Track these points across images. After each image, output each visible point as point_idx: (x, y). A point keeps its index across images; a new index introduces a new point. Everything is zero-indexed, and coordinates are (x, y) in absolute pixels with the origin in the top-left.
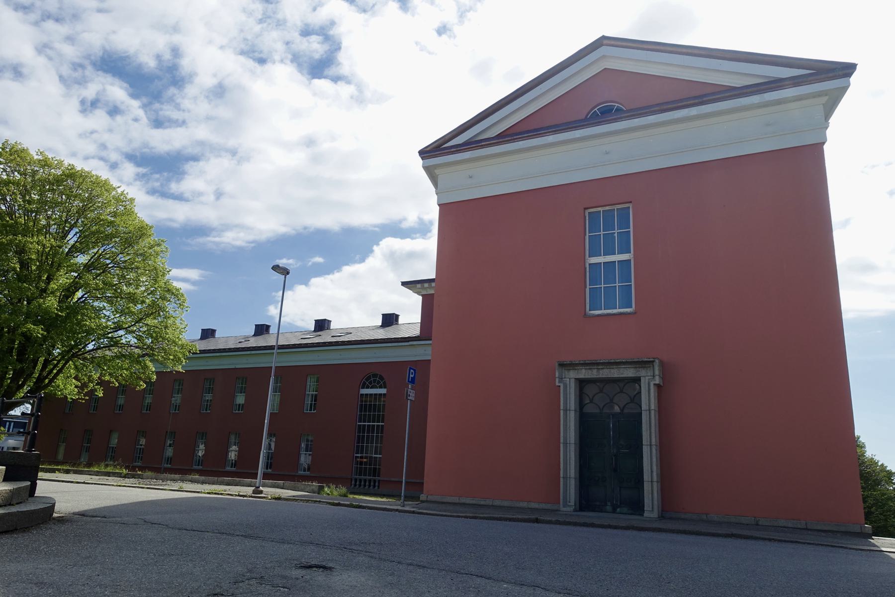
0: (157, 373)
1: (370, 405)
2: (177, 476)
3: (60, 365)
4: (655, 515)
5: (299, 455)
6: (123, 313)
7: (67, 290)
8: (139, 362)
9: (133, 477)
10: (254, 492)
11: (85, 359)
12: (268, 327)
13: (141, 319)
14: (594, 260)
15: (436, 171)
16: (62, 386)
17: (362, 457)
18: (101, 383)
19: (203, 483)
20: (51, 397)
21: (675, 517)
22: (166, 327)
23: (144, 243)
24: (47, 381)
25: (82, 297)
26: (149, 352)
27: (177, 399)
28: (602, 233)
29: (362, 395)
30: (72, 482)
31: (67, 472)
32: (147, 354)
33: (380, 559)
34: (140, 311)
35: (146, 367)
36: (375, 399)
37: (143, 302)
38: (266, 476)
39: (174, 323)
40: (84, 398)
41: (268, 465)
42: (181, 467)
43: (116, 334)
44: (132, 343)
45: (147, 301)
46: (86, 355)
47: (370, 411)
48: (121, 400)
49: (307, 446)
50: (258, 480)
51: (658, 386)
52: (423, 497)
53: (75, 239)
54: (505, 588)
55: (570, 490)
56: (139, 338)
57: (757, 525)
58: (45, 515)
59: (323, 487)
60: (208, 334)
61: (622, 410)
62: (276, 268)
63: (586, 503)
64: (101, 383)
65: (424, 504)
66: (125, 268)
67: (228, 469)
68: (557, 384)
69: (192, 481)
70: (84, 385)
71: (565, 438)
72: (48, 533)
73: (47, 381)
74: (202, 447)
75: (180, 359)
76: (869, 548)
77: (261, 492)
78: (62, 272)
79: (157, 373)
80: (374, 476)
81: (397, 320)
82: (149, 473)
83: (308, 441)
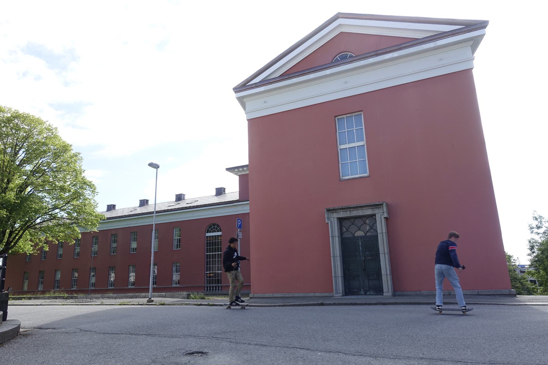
1: (213, 242)
2: (99, 295)
4: (390, 294)
6: (57, 199)
7: (21, 187)
8: (69, 228)
9: (72, 298)
10: (148, 302)
12: (147, 201)
13: (69, 202)
14: (342, 147)
15: (244, 100)
17: (210, 273)
18: (47, 242)
19: (115, 298)
20: (16, 253)
22: (85, 205)
23: (67, 156)
24: (12, 244)
25: (31, 191)
26: (76, 221)
27: (95, 248)
28: (346, 130)
29: (207, 237)
30: (33, 305)
31: (30, 298)
36: (215, 238)
37: (69, 191)
38: (155, 290)
39: (90, 203)
40: (36, 253)
42: (102, 289)
43: (54, 212)
44: (64, 216)
45: (72, 190)
46: (36, 226)
47: (213, 246)
48: (61, 252)
49: (177, 269)
50: (150, 294)
51: (386, 219)
52: (251, 295)
53: (23, 155)
54: (321, 355)
55: (339, 284)
56: (69, 213)
57: (450, 295)
60: (111, 208)
61: (366, 234)
62: (151, 165)
63: (348, 291)
64: (47, 242)
65: (252, 300)
66: (57, 171)
67: (130, 287)
68: (327, 222)
69: (108, 298)
71: (334, 253)
72: (16, 345)
73: (12, 244)
74: (113, 275)
75: (95, 224)
76: (518, 303)
77: (152, 301)
78: (16, 176)
80: (218, 283)
81: (224, 191)
82: (81, 295)
83: (177, 266)
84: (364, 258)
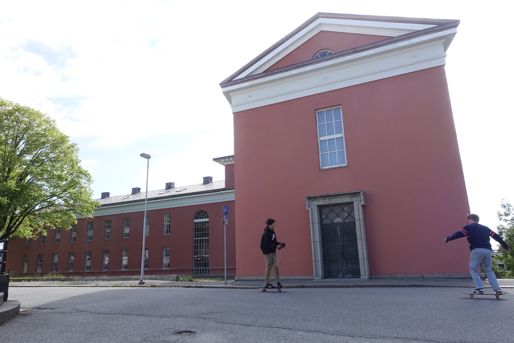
0: (78, 220)
1: (200, 228)
2: (94, 278)
3: (20, 219)
4: (367, 277)
5: (162, 259)
6: (55, 187)
7: (21, 176)
8: (66, 214)
9: (68, 280)
10: (140, 284)
11: (34, 215)
12: (139, 189)
13: (66, 190)
14: (322, 138)
16: (22, 231)
17: (198, 257)
18: (45, 228)
19: (109, 280)
20: (16, 238)
21: (378, 277)
22: (81, 193)
23: (64, 147)
24: (13, 229)
25: (30, 179)
26: (72, 208)
29: (195, 223)
30: (32, 287)
31: (29, 280)
32: (71, 209)
33: (223, 323)
34: (65, 185)
35: (71, 217)
36: (203, 224)
37: (66, 180)
38: (146, 273)
40: (36, 237)
41: (145, 266)
42: (96, 272)
43: (51, 200)
44: (61, 203)
45: (69, 179)
46: (35, 212)
47: (200, 231)
48: (58, 236)
49: (166, 253)
50: (141, 276)
51: (363, 206)
53: (23, 146)
54: (301, 335)
55: (318, 267)
56: (66, 201)
58: (15, 313)
59: (179, 277)
60: (105, 195)
61: (344, 221)
62: (143, 155)
63: (328, 274)
64: (45, 228)
66: (55, 161)
68: (307, 209)
69: (103, 280)
70: (36, 230)
71: (314, 239)
72: (16, 325)
73: (13, 229)
74: (107, 258)
75: (90, 211)
77: (144, 283)
79: (78, 220)
80: (205, 267)
81: (211, 180)
82: (77, 277)
83: (167, 250)
84: (342, 243)
